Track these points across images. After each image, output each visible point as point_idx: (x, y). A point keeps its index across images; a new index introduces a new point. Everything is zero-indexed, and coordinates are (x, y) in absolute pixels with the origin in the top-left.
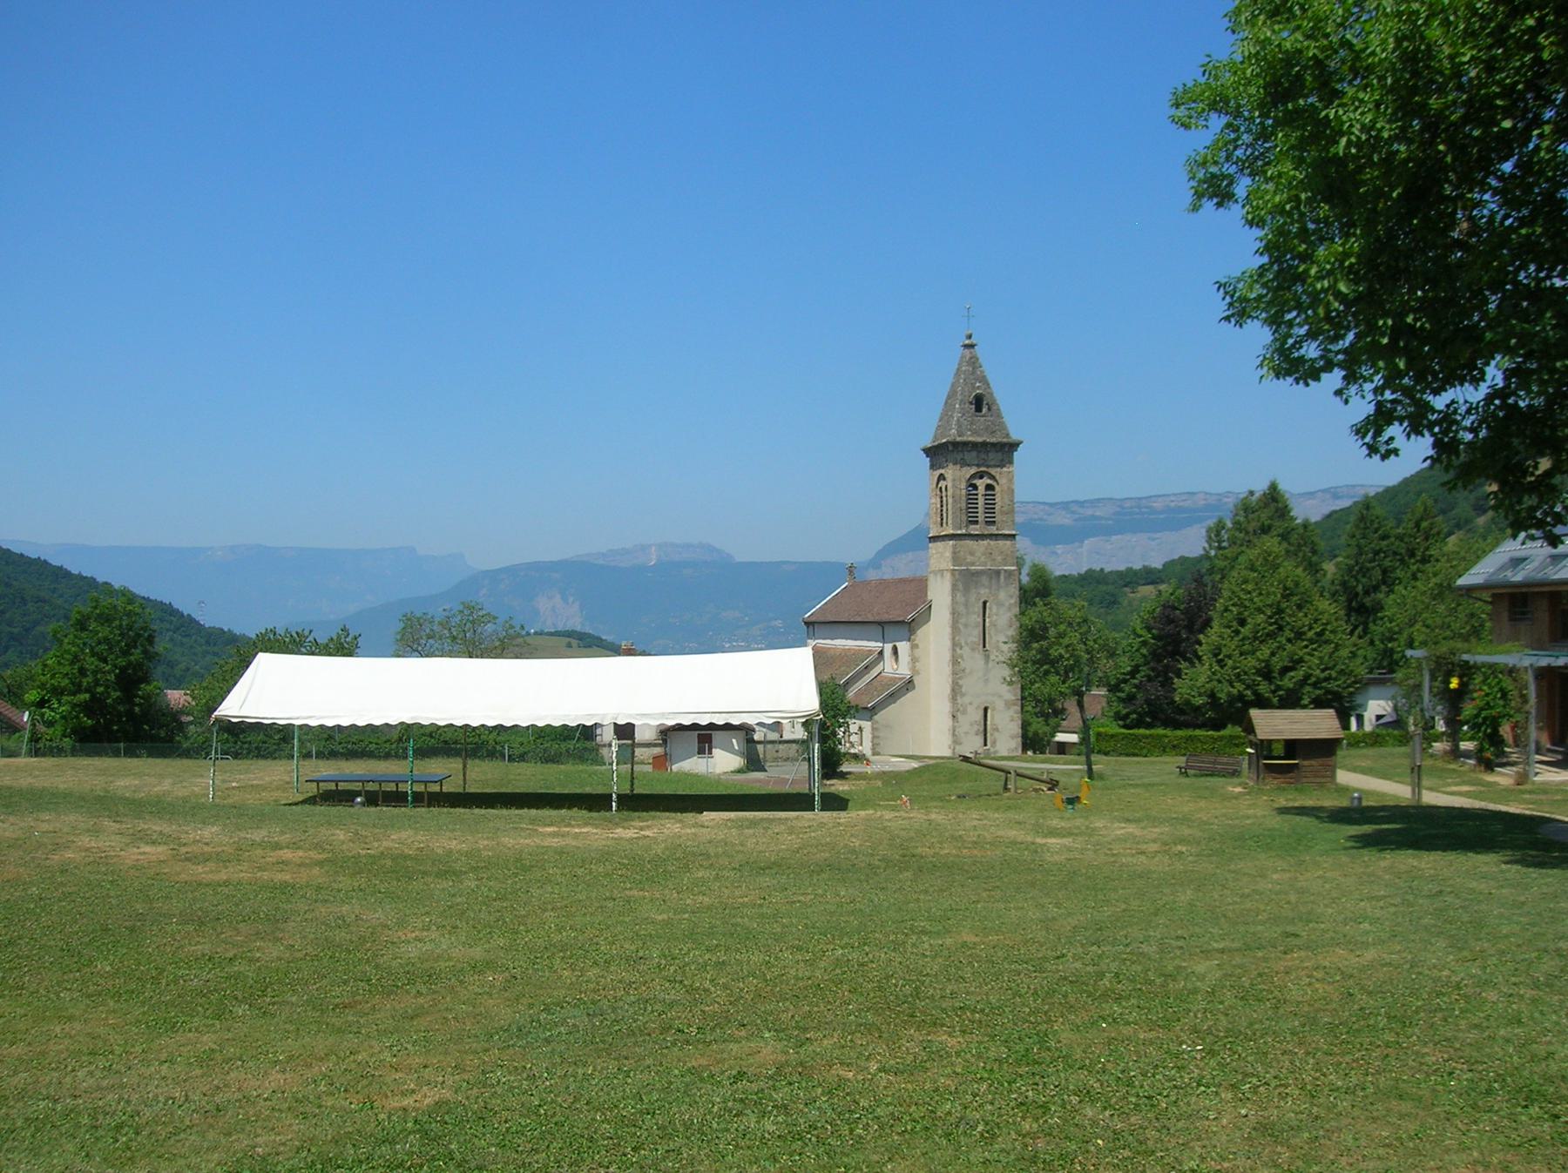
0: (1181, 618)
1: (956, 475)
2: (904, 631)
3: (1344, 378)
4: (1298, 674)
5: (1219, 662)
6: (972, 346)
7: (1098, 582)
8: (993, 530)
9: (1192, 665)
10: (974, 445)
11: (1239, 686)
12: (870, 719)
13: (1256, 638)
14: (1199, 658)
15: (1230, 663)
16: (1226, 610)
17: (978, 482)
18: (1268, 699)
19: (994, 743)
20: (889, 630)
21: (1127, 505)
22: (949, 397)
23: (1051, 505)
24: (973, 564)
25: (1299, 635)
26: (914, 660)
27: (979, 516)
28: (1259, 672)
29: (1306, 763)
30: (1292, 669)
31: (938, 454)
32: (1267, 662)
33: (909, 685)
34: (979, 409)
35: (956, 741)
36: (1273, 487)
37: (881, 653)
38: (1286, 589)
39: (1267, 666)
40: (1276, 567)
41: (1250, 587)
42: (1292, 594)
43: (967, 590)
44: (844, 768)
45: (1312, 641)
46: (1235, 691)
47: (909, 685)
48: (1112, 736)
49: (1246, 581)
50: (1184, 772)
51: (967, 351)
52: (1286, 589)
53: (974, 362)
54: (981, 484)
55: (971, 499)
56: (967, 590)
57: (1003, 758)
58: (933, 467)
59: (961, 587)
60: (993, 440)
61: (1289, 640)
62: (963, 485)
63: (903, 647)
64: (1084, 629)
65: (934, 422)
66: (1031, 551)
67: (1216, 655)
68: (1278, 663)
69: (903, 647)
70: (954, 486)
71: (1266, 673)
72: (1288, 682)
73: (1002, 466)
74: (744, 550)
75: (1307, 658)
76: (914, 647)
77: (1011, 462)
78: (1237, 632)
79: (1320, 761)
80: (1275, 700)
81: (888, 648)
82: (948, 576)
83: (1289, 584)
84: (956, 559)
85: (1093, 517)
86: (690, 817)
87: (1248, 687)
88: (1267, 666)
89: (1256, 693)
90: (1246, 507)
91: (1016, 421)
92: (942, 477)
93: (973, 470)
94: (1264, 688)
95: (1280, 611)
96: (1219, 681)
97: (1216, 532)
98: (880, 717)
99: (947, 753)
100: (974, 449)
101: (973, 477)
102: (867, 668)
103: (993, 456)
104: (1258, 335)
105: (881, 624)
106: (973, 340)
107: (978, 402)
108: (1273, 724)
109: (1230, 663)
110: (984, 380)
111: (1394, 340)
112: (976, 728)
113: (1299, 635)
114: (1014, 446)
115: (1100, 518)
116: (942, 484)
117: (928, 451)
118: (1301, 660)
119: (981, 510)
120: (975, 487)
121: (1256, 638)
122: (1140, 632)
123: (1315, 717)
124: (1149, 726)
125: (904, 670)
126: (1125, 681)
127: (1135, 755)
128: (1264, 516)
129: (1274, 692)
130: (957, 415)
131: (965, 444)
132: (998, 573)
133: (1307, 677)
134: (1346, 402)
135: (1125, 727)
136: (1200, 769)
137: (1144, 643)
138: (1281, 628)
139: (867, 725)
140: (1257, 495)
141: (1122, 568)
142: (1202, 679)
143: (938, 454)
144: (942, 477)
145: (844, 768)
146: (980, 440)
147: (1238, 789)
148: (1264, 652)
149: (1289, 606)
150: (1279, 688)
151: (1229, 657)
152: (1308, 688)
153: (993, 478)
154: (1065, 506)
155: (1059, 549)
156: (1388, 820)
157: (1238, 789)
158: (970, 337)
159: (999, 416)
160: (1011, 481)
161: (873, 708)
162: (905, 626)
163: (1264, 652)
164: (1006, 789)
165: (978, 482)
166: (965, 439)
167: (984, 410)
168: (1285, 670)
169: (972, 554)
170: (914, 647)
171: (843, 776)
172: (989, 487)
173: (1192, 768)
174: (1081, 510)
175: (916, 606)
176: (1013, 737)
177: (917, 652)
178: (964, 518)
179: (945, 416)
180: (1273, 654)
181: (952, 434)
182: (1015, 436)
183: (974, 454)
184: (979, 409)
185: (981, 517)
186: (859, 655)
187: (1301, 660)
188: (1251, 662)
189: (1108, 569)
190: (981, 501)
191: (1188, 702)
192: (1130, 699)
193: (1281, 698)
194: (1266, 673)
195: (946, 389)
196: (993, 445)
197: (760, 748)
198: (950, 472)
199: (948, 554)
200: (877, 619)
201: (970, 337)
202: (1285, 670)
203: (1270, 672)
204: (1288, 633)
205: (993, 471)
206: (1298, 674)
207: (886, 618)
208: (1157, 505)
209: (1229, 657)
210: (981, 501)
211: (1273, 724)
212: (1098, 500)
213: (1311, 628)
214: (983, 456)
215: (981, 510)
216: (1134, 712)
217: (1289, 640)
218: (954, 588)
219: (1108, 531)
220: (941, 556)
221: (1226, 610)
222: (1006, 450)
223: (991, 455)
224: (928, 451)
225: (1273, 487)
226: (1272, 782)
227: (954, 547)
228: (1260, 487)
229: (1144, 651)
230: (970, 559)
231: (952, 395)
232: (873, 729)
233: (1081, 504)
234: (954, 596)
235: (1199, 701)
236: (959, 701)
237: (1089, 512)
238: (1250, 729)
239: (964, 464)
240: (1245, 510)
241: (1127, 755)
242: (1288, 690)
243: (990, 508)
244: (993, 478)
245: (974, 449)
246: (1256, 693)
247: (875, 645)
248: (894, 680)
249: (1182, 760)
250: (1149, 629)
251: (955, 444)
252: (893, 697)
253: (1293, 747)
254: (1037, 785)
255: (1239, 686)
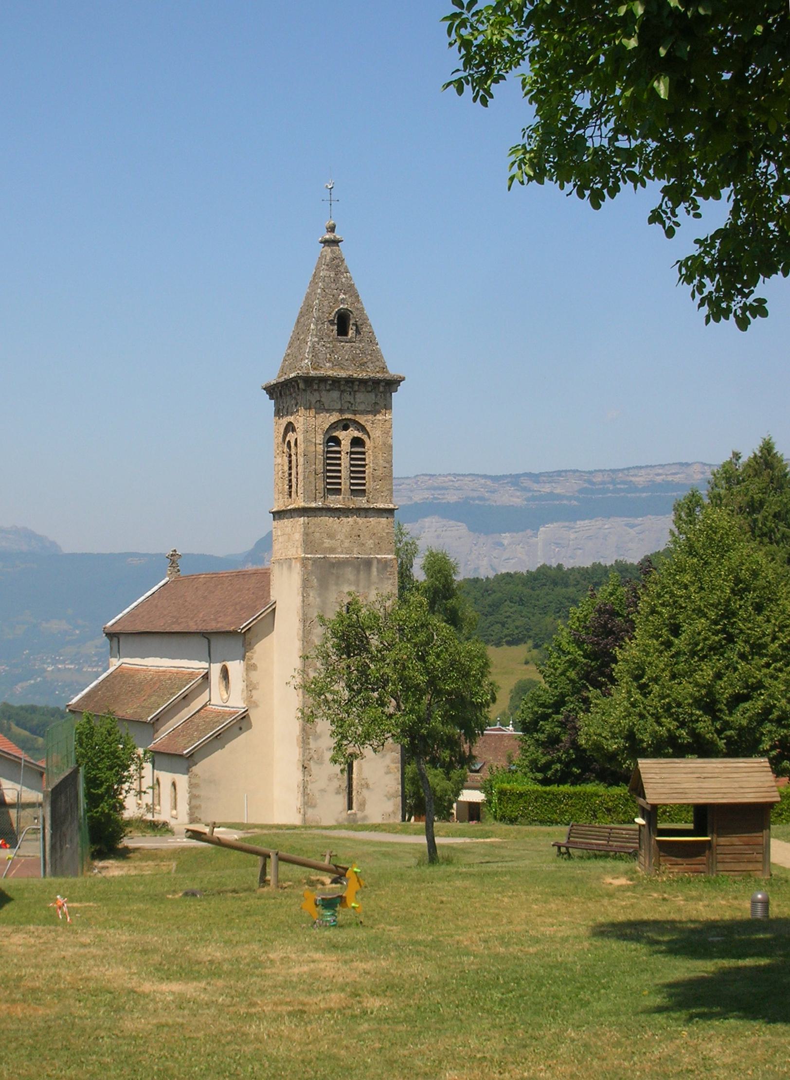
0: (598, 625)
1: (311, 425)
2: (236, 645)
3: (666, 191)
4: (755, 706)
5: (642, 687)
6: (335, 242)
7: (555, 583)
8: (362, 502)
9: (607, 694)
10: (336, 382)
11: (670, 724)
12: (187, 771)
13: (693, 653)
14: (613, 681)
15: (656, 688)
16: (653, 612)
17: (342, 435)
18: (712, 743)
19: (363, 805)
20: (218, 644)
21: (598, 479)
22: (301, 315)
23: (495, 479)
24: (332, 550)
25: (758, 648)
26: (250, 687)
27: (341, 481)
28: (697, 702)
29: (722, 840)
30: (746, 698)
31: (285, 393)
32: (710, 687)
33: (243, 722)
34: (343, 330)
35: (308, 801)
36: (768, 448)
37: (206, 677)
38: (738, 580)
39: (710, 694)
40: (724, 550)
41: (687, 578)
42: (747, 589)
43: (323, 586)
44: (127, 842)
45: (775, 658)
46: (663, 731)
47: (243, 722)
48: (521, 795)
49: (682, 570)
50: (564, 852)
51: (328, 249)
52: (738, 580)
53: (337, 265)
54: (346, 437)
55: (331, 459)
56: (323, 586)
57: (375, 828)
58: (279, 413)
59: (315, 582)
60: (363, 375)
61: (742, 656)
62: (320, 439)
63: (236, 667)
64: (422, 636)
65: (282, 349)
66: (431, 536)
67: (637, 678)
68: (724, 691)
69: (236, 667)
70: (306, 440)
71: (709, 705)
72: (740, 717)
73: (375, 412)
74: (72, 541)
75: (767, 682)
76: (250, 668)
77: (388, 407)
78: (668, 644)
79: (746, 837)
80: (721, 744)
81: (216, 669)
82: (297, 567)
83: (744, 574)
84: (308, 543)
85: (552, 496)
86: (291, 865)
87: (682, 724)
88: (710, 694)
89: (693, 733)
90: (729, 476)
91: (395, 347)
92: (290, 427)
93: (334, 418)
94: (705, 725)
95: (729, 614)
96: (642, 716)
97: (688, 508)
98: (201, 768)
99: (295, 819)
100: (337, 389)
101: (334, 426)
102: (186, 699)
103: (363, 398)
104: (513, 108)
105: (206, 635)
106: (337, 235)
107: (343, 322)
108: (676, 782)
109: (656, 688)
110: (350, 290)
111: (648, 43)
112: (336, 783)
113: (758, 648)
114: (392, 384)
115: (559, 497)
116: (291, 437)
117: (276, 391)
118: (760, 685)
119: (345, 473)
120: (337, 441)
121: (693, 653)
122: (565, 646)
123: (737, 770)
124: (577, 780)
125: (236, 701)
126: (545, 717)
127: (552, 822)
128: (754, 488)
129: (719, 732)
130: (311, 339)
131: (323, 380)
132: (368, 563)
133: (767, 711)
134: (670, 233)
135: (545, 782)
136: (588, 847)
137: (573, 663)
138: (730, 639)
139: (182, 780)
140: (744, 459)
141: (588, 564)
142: (619, 712)
143: (285, 393)
144: (290, 427)
145: (127, 842)
146: (343, 374)
147: (623, 881)
148: (706, 673)
149: (743, 606)
150: (727, 725)
151: (656, 680)
152: (768, 726)
153: (362, 428)
154: (515, 480)
155: (506, 538)
156: (762, 949)
157: (623, 881)
158: (332, 229)
159: (372, 341)
160: (387, 433)
161: (191, 755)
162: (234, 638)
163: (706, 673)
164: (263, 881)
165: (342, 435)
166: (321, 373)
167: (351, 333)
168: (737, 699)
169: (331, 536)
170: (250, 668)
171: (124, 854)
172: (357, 442)
173: (576, 846)
174: (535, 487)
175: (254, 609)
176: (389, 797)
177: (254, 676)
178: (321, 485)
179: (297, 341)
180: (719, 676)
181: (305, 367)
182: (394, 370)
183: (335, 394)
184: (343, 330)
185: (345, 485)
186: (177, 679)
187: (760, 685)
188: (685, 690)
189: (568, 565)
190: (345, 461)
191: (598, 747)
192: (553, 741)
193: (729, 741)
194: (709, 705)
195: (299, 303)
196: (363, 382)
197: (13, 813)
198: (301, 419)
199: (298, 536)
200: (201, 628)
201: (332, 229)
202: (737, 699)
203: (715, 702)
204: (741, 646)
205: (361, 419)
206: (755, 706)
207: (212, 626)
208: (640, 480)
209: (656, 680)
210: (345, 461)
211: (676, 782)
212: (559, 473)
213: (774, 638)
214: (347, 397)
215: (345, 473)
216: (559, 760)
217: (742, 656)
218: (306, 584)
219: (572, 515)
220: (290, 538)
221: (653, 612)
222: (382, 389)
223: (360, 397)
224: (276, 391)
225: (768, 448)
226: (672, 870)
227: (306, 526)
228: (749, 450)
229: (572, 674)
230: (328, 543)
231: (305, 312)
232: (192, 786)
233: (535, 477)
234: (305, 597)
235: (613, 746)
236: (313, 745)
237: (547, 489)
238: (638, 790)
239: (321, 408)
240: (728, 480)
241: (542, 822)
242: (741, 729)
243: (358, 471)
244: (362, 428)
245: (337, 389)
246: (693, 733)
247: (198, 666)
248: (221, 715)
249: (560, 833)
250: (579, 643)
251: (309, 382)
252: (220, 739)
253: (707, 816)
254: (315, 876)
255: (670, 724)
